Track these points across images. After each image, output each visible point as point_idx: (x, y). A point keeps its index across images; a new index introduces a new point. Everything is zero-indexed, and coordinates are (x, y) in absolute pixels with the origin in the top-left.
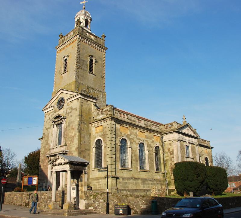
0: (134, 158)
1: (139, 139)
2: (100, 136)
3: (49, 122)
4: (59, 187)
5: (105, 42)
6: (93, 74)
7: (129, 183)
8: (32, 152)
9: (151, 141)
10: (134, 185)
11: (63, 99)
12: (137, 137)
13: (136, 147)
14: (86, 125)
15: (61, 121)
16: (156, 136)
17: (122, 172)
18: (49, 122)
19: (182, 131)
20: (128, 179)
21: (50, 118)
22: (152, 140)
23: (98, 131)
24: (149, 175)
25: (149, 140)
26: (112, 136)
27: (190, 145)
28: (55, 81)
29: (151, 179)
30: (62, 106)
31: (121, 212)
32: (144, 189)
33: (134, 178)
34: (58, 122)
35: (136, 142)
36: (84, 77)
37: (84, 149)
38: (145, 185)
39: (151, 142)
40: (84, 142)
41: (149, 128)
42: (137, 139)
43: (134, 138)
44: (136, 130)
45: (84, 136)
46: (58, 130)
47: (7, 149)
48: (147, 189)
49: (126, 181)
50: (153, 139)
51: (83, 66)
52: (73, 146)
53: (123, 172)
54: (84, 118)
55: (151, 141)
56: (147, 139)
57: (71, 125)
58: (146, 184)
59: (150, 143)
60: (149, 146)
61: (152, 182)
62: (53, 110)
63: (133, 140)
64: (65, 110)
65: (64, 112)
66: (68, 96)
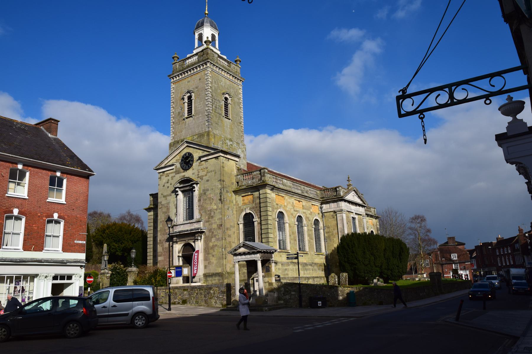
0: (292, 237)
1: (296, 211)
3: (168, 187)
5: (465, 246)
6: (230, 119)
9: (309, 212)
10: (294, 271)
12: (294, 208)
13: (295, 221)
16: (315, 205)
17: (281, 256)
21: (168, 180)
22: (310, 211)
23: (246, 201)
24: (309, 258)
25: (306, 211)
26: (269, 209)
27: (356, 217)
28: (171, 126)
29: (311, 263)
31: (320, 304)
32: (305, 276)
37: (229, 226)
38: (306, 272)
39: (309, 213)
41: (306, 194)
42: (294, 211)
44: (292, 199)
48: (307, 276)
50: (311, 210)
53: (282, 255)
54: (226, 184)
56: (304, 211)
57: (208, 193)
58: (306, 270)
59: (308, 215)
60: (307, 218)
61: (312, 268)
62: (174, 170)
63: (290, 212)
64: (195, 171)
65: (193, 174)
66: (201, 153)
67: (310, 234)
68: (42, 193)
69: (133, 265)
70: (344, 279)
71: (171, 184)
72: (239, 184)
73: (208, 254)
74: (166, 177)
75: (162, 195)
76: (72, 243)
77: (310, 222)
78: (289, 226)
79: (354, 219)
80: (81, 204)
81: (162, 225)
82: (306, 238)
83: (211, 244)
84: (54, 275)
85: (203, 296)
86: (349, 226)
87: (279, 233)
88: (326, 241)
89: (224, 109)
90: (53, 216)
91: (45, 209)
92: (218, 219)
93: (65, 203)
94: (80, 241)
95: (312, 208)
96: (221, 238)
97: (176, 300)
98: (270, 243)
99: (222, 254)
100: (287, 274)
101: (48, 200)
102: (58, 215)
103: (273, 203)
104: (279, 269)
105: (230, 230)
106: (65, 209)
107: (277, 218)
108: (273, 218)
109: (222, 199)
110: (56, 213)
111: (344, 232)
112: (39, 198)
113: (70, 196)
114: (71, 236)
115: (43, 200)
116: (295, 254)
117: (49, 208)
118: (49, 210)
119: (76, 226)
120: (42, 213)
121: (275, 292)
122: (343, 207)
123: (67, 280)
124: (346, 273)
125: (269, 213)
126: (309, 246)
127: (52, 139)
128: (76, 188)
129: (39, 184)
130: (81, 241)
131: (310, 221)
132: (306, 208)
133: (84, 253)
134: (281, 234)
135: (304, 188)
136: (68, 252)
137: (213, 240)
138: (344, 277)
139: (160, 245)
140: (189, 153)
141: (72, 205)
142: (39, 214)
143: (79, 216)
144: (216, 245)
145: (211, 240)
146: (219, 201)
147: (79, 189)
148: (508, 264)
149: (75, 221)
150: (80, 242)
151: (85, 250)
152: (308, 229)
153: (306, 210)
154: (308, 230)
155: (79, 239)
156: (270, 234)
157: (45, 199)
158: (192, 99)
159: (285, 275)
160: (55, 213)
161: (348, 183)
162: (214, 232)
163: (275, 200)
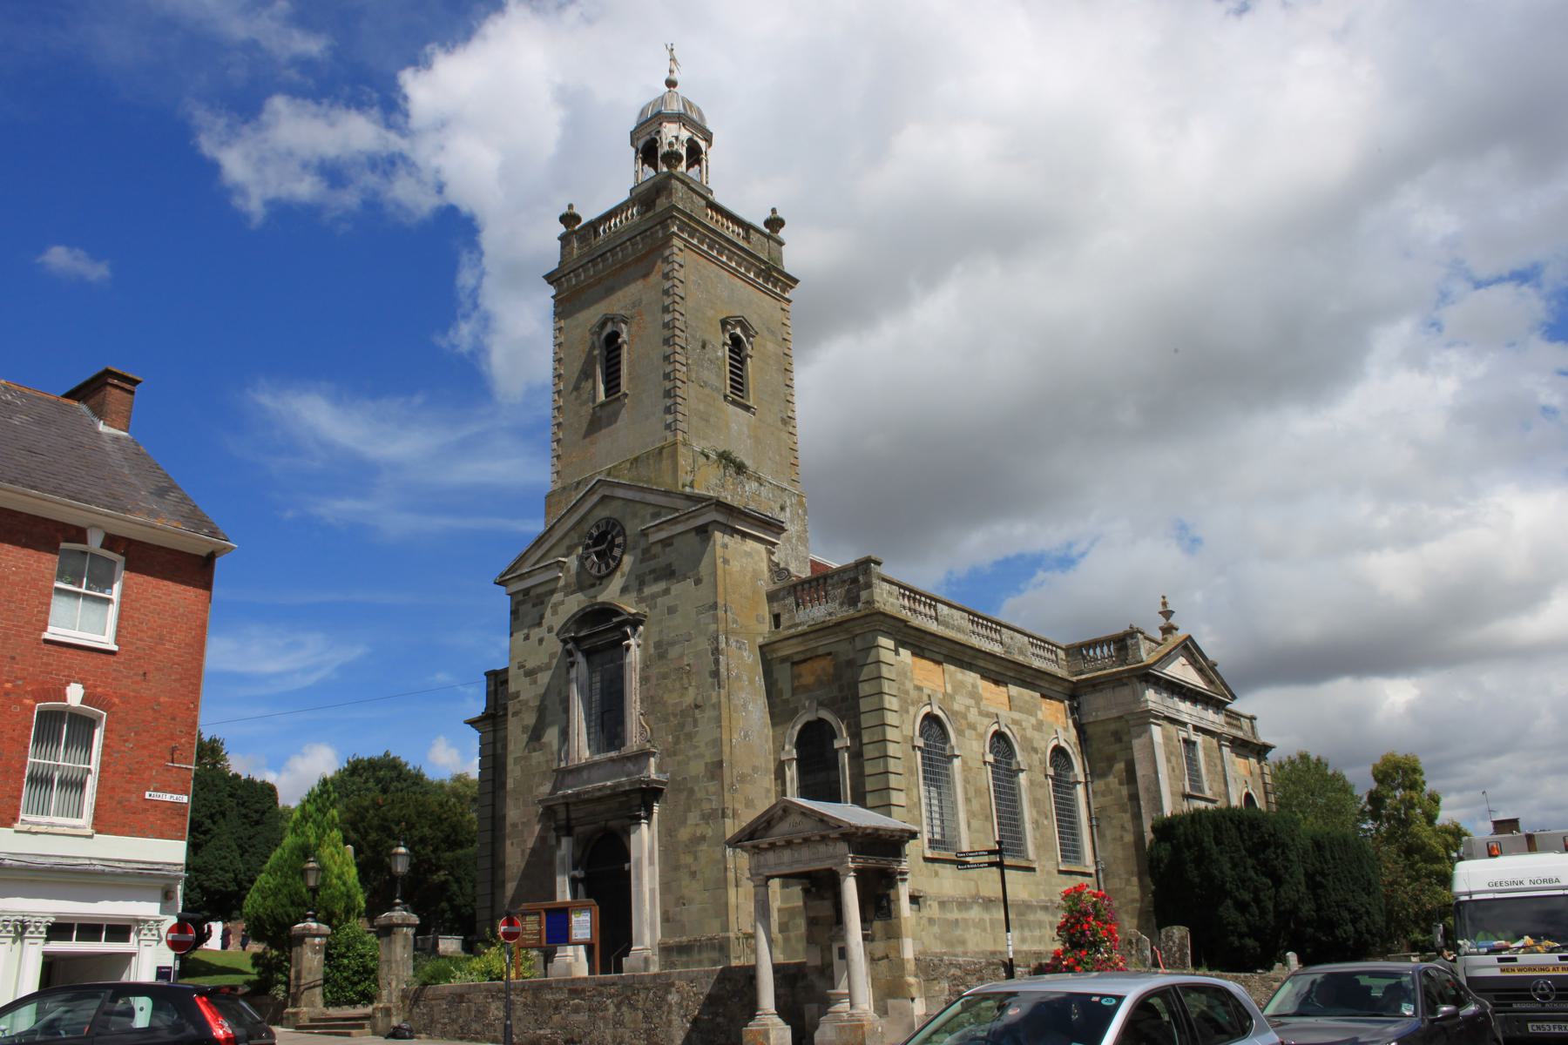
0: (975, 805)
2: (821, 704)
3: (541, 641)
4: (627, 955)
7: (965, 920)
8: (348, 762)
9: (1033, 720)
10: (985, 930)
11: (614, 526)
12: (978, 704)
14: (745, 654)
15: (616, 636)
17: (937, 874)
18: (541, 641)
19: (1165, 671)
20: (963, 905)
23: (808, 679)
26: (890, 702)
27: (1199, 739)
30: (612, 564)
33: (983, 898)
34: (599, 642)
35: (974, 729)
36: (712, 420)
37: (747, 770)
38: (1027, 933)
39: (1033, 726)
40: (746, 735)
43: (968, 708)
45: (745, 706)
46: (597, 678)
47: (1289, 757)
49: (955, 915)
51: (702, 366)
52: (691, 753)
54: (735, 621)
55: (1033, 720)
56: (1016, 715)
57: (673, 652)
59: (1030, 733)
63: (966, 719)
67: (1039, 800)
68: (23, 609)
69: (398, 901)
70: (1175, 949)
71: (550, 630)
72: (782, 620)
73: (677, 868)
74: (534, 606)
75: (519, 668)
76: (134, 798)
77: (1036, 757)
78: (963, 766)
79: (1189, 743)
80: (178, 656)
81: (522, 771)
82: (1028, 813)
83: (684, 834)
84: (53, 920)
85: (641, 1015)
86: (1173, 770)
87: (929, 792)
88: (1094, 823)
89: (728, 372)
90: (65, 695)
91: (33, 667)
92: (706, 744)
93: (115, 648)
94: (169, 795)
95: (1043, 708)
96: (720, 812)
97: (542, 1032)
98: (892, 808)
99: (722, 866)
100: (963, 942)
101: (46, 636)
102: (82, 691)
103: (903, 684)
104: (931, 921)
105: (703, 711)
106: (115, 670)
107: (921, 735)
108: (905, 737)
109: (723, 670)
110: (77, 682)
111: (1161, 809)
112: (14, 626)
113: (134, 625)
114: (130, 773)
115: (29, 633)
116: (991, 852)
117: (47, 664)
118: (48, 673)
119: (152, 736)
120: (20, 682)
121: (913, 999)
122: (1150, 704)
123: (106, 941)
124: (1182, 927)
125: (891, 718)
126: (1036, 839)
127: (106, 438)
128: (160, 598)
129: (15, 573)
130: (170, 792)
131: (1035, 750)
132: (1021, 707)
133: (181, 838)
134: (934, 794)
135: (1012, 638)
136: (116, 834)
137: (693, 817)
138: (1177, 941)
139: (515, 841)
140: (608, 520)
141: (139, 658)
142: (9, 685)
143: (167, 699)
144: (703, 838)
145: (686, 819)
146: (710, 680)
147: (172, 600)
148: (1529, 1025)
149: (150, 719)
150: (167, 797)
151: (184, 829)
152: (1033, 785)
153: (1020, 712)
154: (1032, 783)
155: (164, 786)
156: (894, 793)
157: (35, 630)
158: (620, 340)
159: (951, 944)
160: (72, 684)
161: (1162, 621)
162: (696, 788)
163: (912, 672)
